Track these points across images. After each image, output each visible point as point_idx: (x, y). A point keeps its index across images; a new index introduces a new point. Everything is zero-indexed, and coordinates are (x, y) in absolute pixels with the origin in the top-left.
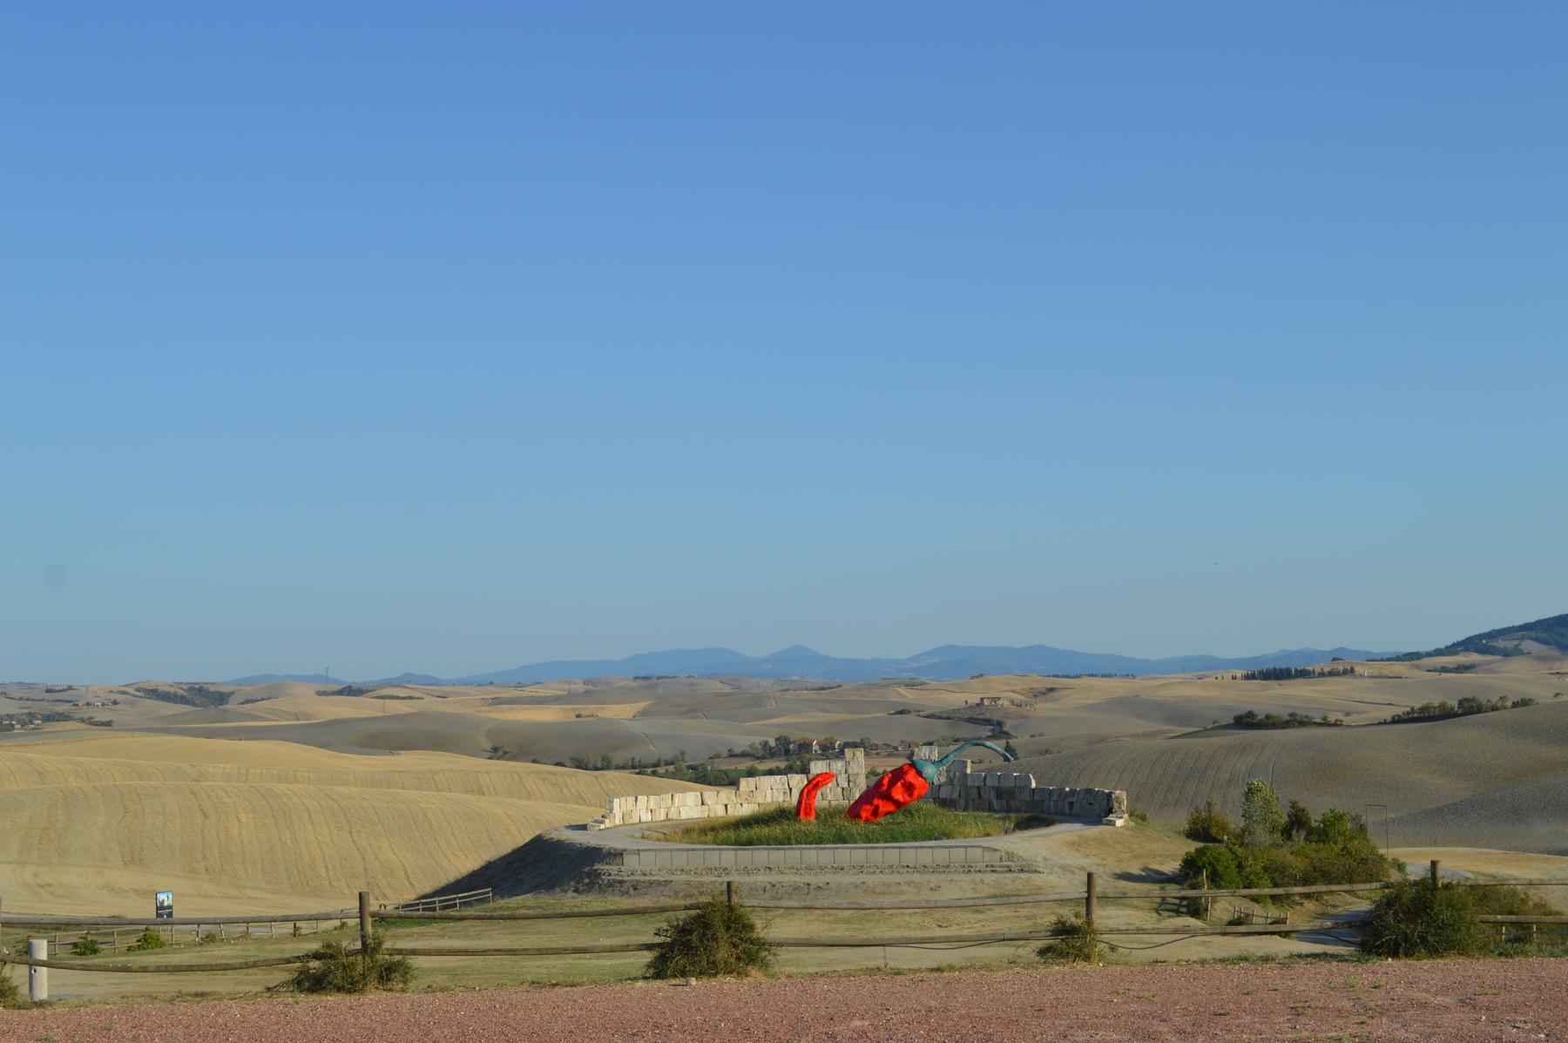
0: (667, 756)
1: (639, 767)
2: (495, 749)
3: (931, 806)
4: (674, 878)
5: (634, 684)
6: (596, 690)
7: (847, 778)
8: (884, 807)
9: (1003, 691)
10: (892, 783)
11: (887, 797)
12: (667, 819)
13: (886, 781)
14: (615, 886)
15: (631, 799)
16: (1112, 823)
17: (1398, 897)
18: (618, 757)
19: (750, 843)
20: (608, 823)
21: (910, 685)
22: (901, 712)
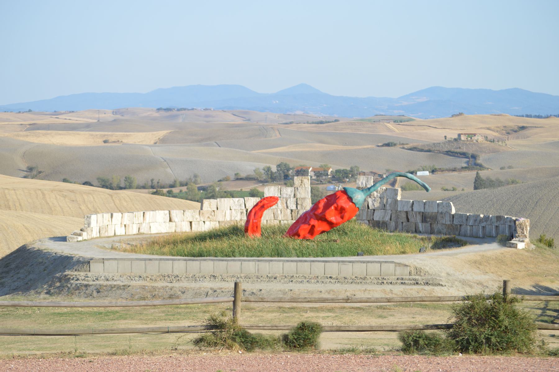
0: (183, 179)
1: (156, 188)
2: (31, 169)
3: (365, 227)
4: (133, 283)
5: (156, 115)
6: (122, 120)
7: (289, 203)
8: (320, 226)
9: (479, 128)
10: (327, 206)
11: (322, 218)
12: (139, 233)
13: (321, 205)
14: (82, 289)
15: (107, 216)
16: (514, 246)
17: (472, 307)
18: (139, 178)
19: (200, 255)
20: (85, 236)
21: (398, 121)
22: (388, 145)
